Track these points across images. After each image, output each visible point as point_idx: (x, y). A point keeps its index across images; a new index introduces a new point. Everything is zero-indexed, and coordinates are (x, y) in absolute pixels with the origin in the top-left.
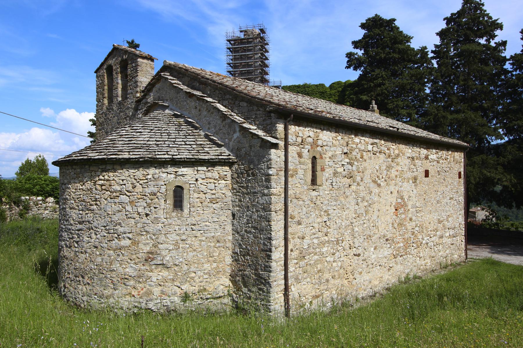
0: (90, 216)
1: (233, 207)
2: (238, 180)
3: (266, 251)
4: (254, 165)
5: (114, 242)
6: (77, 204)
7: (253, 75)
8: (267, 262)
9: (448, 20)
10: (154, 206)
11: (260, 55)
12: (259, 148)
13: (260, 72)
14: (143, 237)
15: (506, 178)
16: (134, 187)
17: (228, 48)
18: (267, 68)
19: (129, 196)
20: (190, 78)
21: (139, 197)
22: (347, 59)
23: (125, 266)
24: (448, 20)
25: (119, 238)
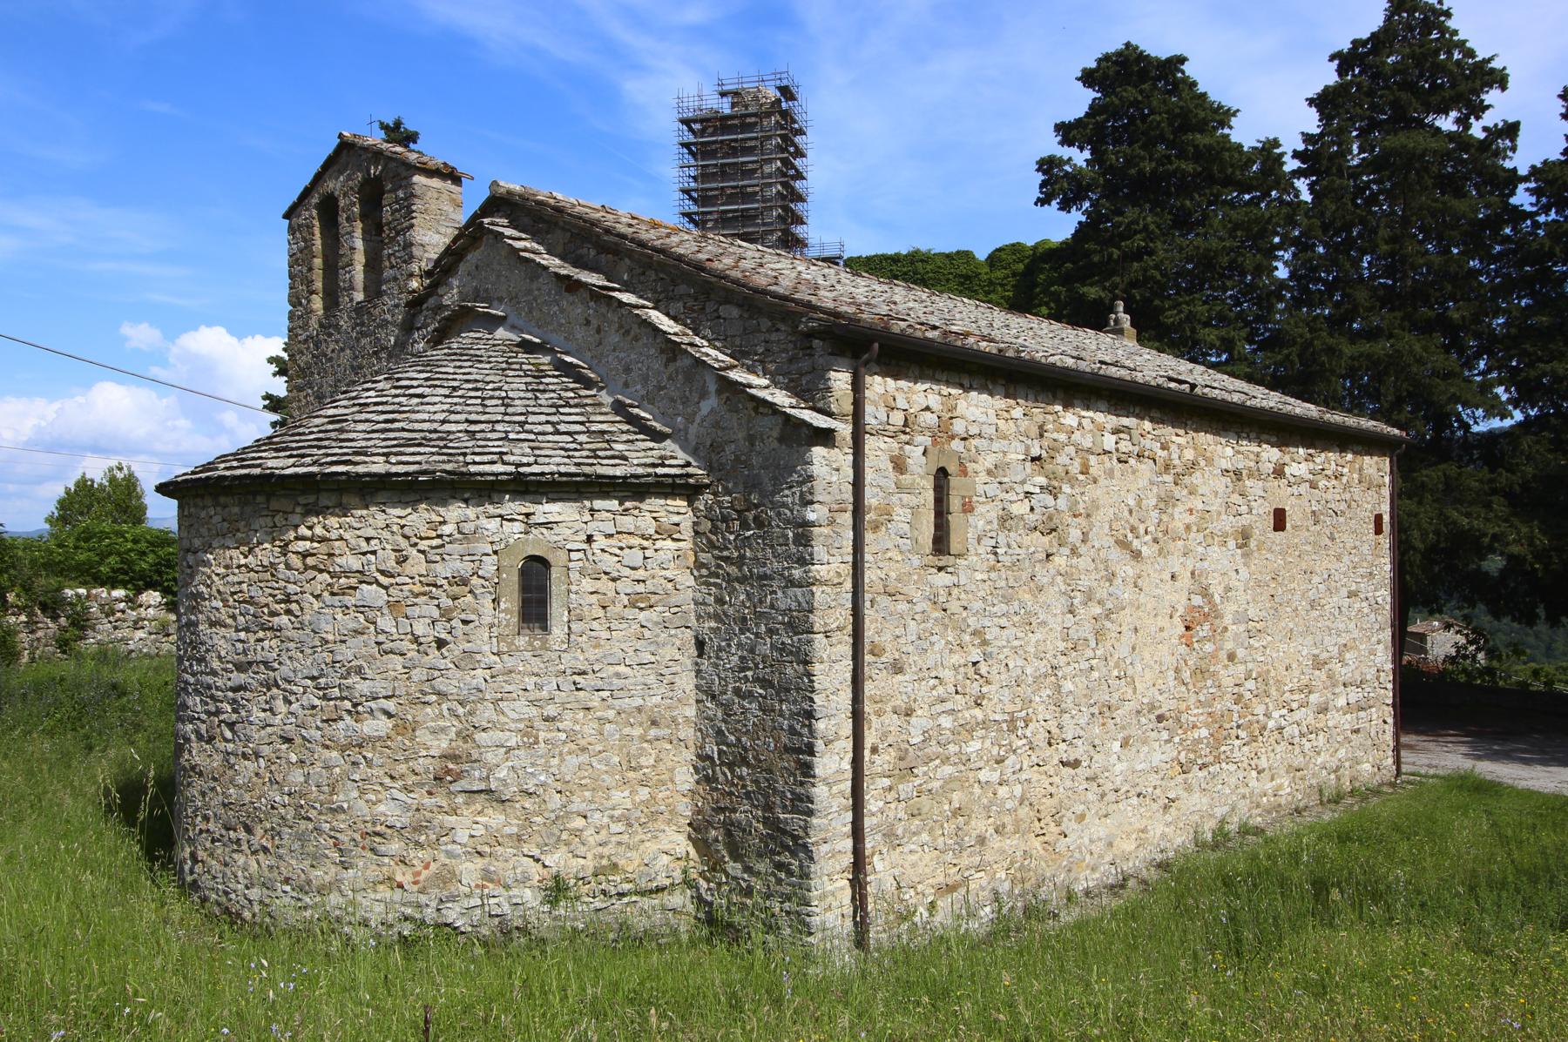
0: (269, 648)
1: (698, 620)
2: (714, 538)
3: (799, 751)
4: (763, 495)
5: (341, 724)
6: (231, 610)
7: (758, 225)
8: (802, 784)
9: (1344, 61)
10: (463, 616)
11: (779, 163)
12: (776, 444)
13: (779, 216)
14: (428, 710)
15: (1518, 534)
16: (402, 560)
17: (684, 145)
18: (800, 205)
19: (386, 588)
20: (568, 234)
21: (418, 588)
22: (1040, 177)
23: (373, 798)
24: (1344, 61)
25: (357, 712)
